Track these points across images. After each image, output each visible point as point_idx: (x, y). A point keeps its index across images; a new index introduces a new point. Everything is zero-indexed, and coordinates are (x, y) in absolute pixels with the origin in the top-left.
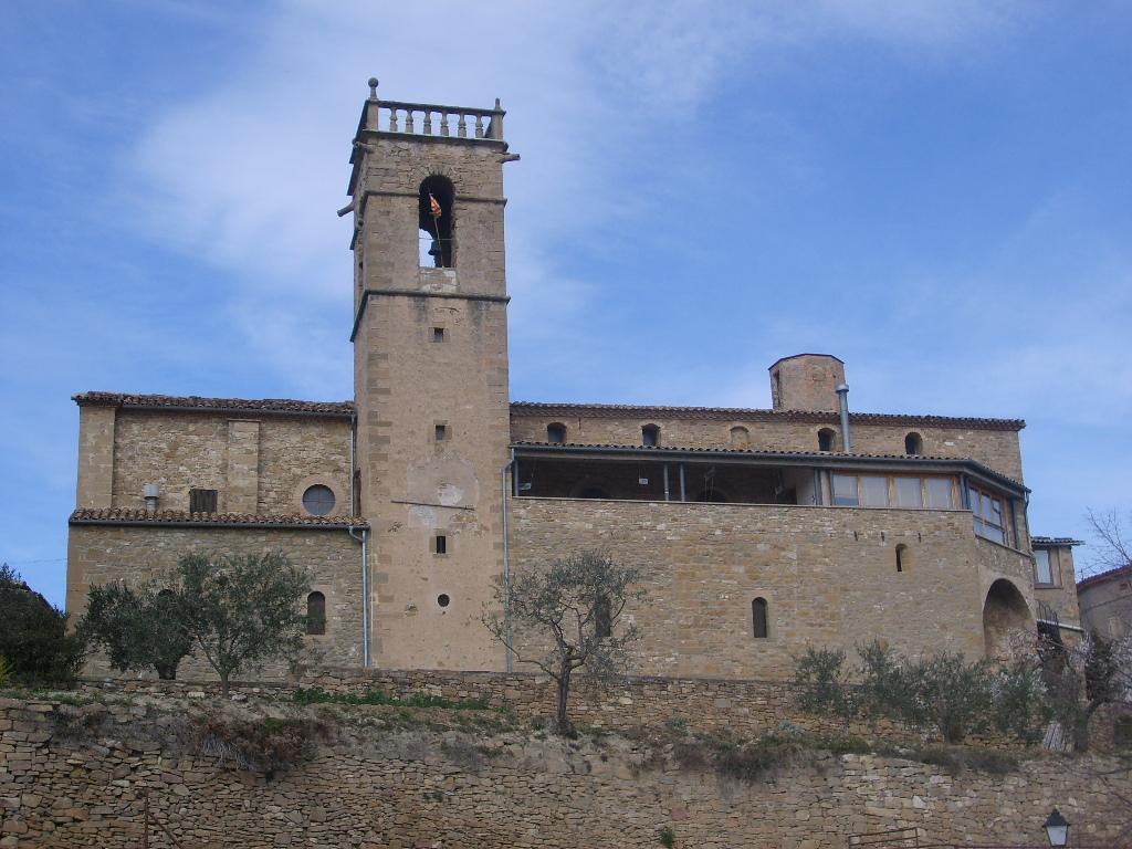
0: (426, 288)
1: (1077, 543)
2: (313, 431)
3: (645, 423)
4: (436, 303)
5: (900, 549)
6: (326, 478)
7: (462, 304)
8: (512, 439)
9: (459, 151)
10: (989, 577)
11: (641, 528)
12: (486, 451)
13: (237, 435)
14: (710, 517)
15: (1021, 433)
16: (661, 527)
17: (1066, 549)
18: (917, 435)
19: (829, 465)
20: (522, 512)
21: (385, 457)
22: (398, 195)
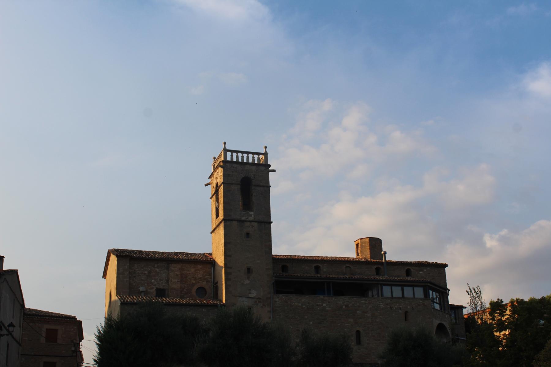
0: (243, 218)
1: (465, 308)
2: (200, 267)
3: (315, 265)
4: (247, 224)
5: (406, 313)
6: (204, 284)
7: (255, 224)
8: (274, 273)
9: (254, 168)
10: (436, 322)
11: (317, 305)
13: (173, 269)
14: (341, 301)
15: (446, 269)
16: (325, 305)
18: (410, 269)
19: (381, 283)
20: (277, 300)
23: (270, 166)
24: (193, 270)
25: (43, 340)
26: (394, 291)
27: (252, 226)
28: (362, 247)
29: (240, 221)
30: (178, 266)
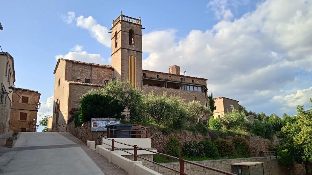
0: (130, 49)
2: (106, 70)
4: (132, 51)
5: (196, 97)
9: (135, 26)
12: (140, 77)
15: (207, 81)
17: (113, 162)
19: (186, 84)
21: (123, 77)
22: (125, 32)
23: (142, 26)
24: (103, 71)
25: (20, 101)
26: (190, 88)
27: (134, 53)
28: (172, 69)
29: (128, 49)
30: (97, 69)
